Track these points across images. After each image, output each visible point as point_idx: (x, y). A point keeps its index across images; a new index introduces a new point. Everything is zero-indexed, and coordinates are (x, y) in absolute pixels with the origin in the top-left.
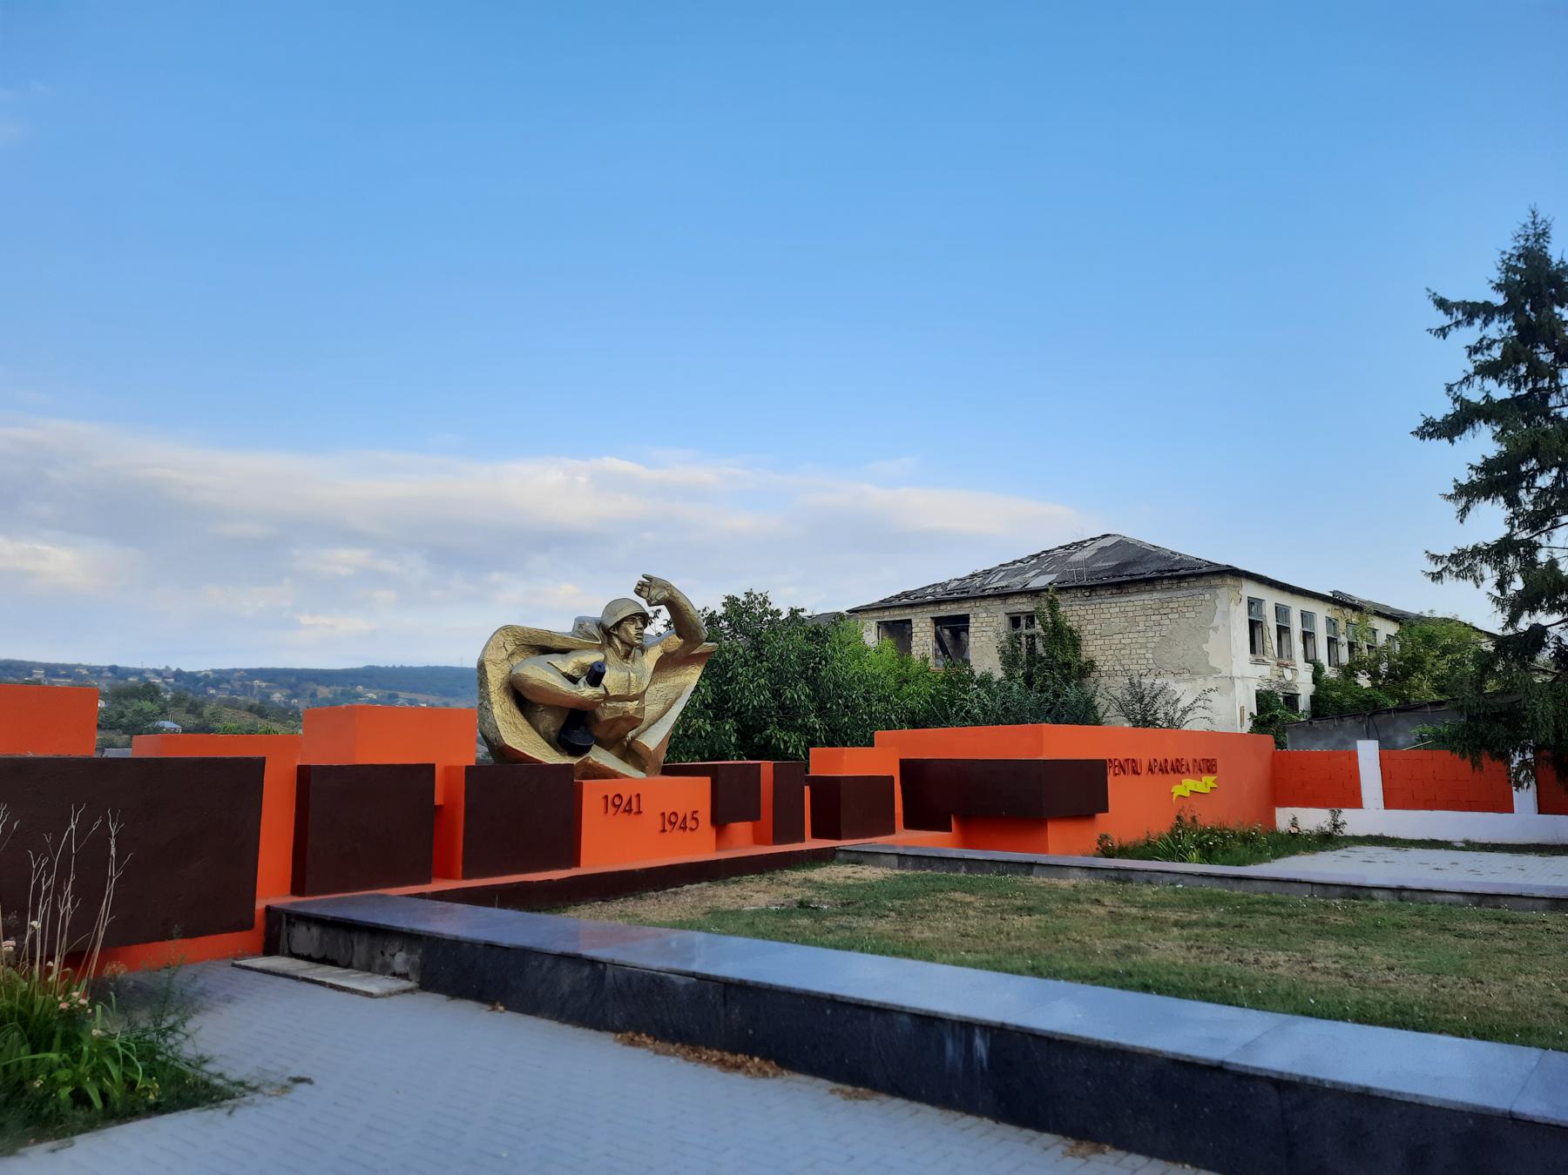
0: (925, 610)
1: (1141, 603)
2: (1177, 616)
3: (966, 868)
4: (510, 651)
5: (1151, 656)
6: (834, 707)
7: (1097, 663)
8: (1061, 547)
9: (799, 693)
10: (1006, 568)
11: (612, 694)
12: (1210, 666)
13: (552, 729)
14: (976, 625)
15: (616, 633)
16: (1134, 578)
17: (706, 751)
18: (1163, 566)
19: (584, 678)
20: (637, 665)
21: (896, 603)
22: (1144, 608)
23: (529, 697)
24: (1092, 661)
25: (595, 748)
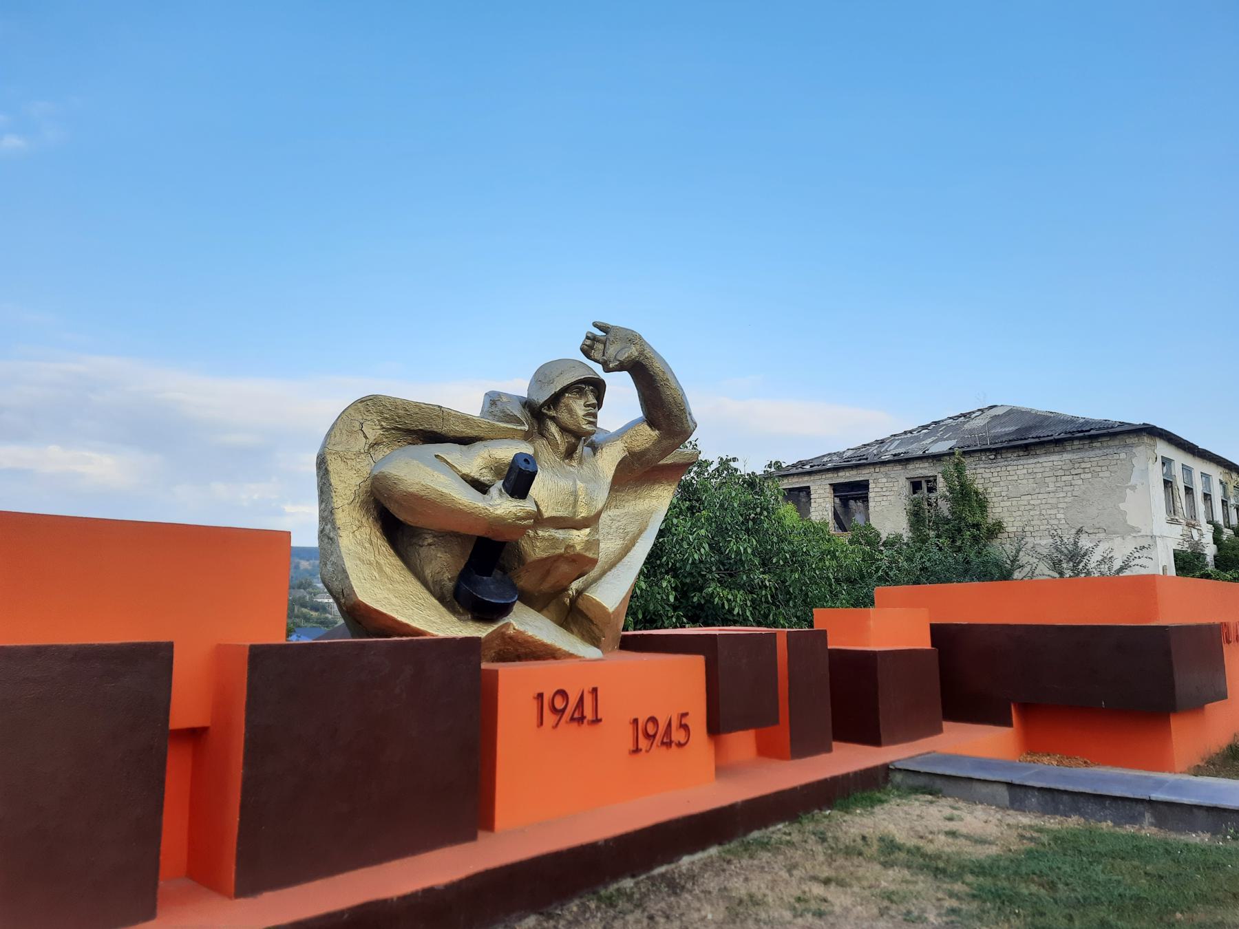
0: (824, 477)
1: (1051, 464)
2: (1090, 475)
3: (1154, 815)
4: (371, 439)
5: (1062, 516)
6: (781, 563)
7: (1005, 525)
8: (950, 418)
9: (743, 546)
10: (899, 437)
11: (546, 515)
12: (1128, 525)
13: (447, 575)
14: (876, 490)
15: (552, 413)
16: (1042, 439)
17: (640, 612)
18: (1069, 428)
19: (499, 484)
20: (586, 470)
21: (794, 471)
22: (1053, 469)
23: (402, 516)
24: (1000, 522)
25: (518, 607)
